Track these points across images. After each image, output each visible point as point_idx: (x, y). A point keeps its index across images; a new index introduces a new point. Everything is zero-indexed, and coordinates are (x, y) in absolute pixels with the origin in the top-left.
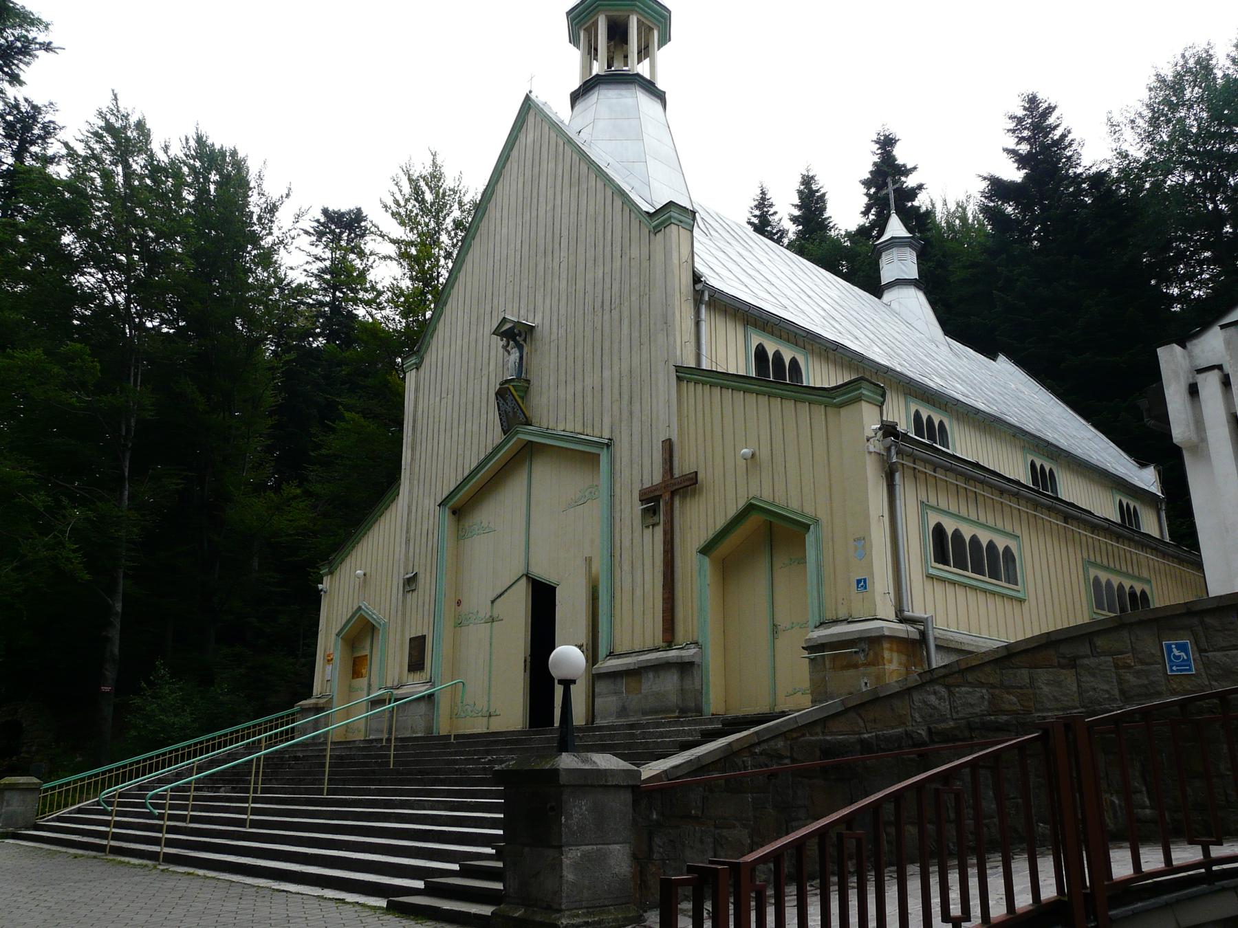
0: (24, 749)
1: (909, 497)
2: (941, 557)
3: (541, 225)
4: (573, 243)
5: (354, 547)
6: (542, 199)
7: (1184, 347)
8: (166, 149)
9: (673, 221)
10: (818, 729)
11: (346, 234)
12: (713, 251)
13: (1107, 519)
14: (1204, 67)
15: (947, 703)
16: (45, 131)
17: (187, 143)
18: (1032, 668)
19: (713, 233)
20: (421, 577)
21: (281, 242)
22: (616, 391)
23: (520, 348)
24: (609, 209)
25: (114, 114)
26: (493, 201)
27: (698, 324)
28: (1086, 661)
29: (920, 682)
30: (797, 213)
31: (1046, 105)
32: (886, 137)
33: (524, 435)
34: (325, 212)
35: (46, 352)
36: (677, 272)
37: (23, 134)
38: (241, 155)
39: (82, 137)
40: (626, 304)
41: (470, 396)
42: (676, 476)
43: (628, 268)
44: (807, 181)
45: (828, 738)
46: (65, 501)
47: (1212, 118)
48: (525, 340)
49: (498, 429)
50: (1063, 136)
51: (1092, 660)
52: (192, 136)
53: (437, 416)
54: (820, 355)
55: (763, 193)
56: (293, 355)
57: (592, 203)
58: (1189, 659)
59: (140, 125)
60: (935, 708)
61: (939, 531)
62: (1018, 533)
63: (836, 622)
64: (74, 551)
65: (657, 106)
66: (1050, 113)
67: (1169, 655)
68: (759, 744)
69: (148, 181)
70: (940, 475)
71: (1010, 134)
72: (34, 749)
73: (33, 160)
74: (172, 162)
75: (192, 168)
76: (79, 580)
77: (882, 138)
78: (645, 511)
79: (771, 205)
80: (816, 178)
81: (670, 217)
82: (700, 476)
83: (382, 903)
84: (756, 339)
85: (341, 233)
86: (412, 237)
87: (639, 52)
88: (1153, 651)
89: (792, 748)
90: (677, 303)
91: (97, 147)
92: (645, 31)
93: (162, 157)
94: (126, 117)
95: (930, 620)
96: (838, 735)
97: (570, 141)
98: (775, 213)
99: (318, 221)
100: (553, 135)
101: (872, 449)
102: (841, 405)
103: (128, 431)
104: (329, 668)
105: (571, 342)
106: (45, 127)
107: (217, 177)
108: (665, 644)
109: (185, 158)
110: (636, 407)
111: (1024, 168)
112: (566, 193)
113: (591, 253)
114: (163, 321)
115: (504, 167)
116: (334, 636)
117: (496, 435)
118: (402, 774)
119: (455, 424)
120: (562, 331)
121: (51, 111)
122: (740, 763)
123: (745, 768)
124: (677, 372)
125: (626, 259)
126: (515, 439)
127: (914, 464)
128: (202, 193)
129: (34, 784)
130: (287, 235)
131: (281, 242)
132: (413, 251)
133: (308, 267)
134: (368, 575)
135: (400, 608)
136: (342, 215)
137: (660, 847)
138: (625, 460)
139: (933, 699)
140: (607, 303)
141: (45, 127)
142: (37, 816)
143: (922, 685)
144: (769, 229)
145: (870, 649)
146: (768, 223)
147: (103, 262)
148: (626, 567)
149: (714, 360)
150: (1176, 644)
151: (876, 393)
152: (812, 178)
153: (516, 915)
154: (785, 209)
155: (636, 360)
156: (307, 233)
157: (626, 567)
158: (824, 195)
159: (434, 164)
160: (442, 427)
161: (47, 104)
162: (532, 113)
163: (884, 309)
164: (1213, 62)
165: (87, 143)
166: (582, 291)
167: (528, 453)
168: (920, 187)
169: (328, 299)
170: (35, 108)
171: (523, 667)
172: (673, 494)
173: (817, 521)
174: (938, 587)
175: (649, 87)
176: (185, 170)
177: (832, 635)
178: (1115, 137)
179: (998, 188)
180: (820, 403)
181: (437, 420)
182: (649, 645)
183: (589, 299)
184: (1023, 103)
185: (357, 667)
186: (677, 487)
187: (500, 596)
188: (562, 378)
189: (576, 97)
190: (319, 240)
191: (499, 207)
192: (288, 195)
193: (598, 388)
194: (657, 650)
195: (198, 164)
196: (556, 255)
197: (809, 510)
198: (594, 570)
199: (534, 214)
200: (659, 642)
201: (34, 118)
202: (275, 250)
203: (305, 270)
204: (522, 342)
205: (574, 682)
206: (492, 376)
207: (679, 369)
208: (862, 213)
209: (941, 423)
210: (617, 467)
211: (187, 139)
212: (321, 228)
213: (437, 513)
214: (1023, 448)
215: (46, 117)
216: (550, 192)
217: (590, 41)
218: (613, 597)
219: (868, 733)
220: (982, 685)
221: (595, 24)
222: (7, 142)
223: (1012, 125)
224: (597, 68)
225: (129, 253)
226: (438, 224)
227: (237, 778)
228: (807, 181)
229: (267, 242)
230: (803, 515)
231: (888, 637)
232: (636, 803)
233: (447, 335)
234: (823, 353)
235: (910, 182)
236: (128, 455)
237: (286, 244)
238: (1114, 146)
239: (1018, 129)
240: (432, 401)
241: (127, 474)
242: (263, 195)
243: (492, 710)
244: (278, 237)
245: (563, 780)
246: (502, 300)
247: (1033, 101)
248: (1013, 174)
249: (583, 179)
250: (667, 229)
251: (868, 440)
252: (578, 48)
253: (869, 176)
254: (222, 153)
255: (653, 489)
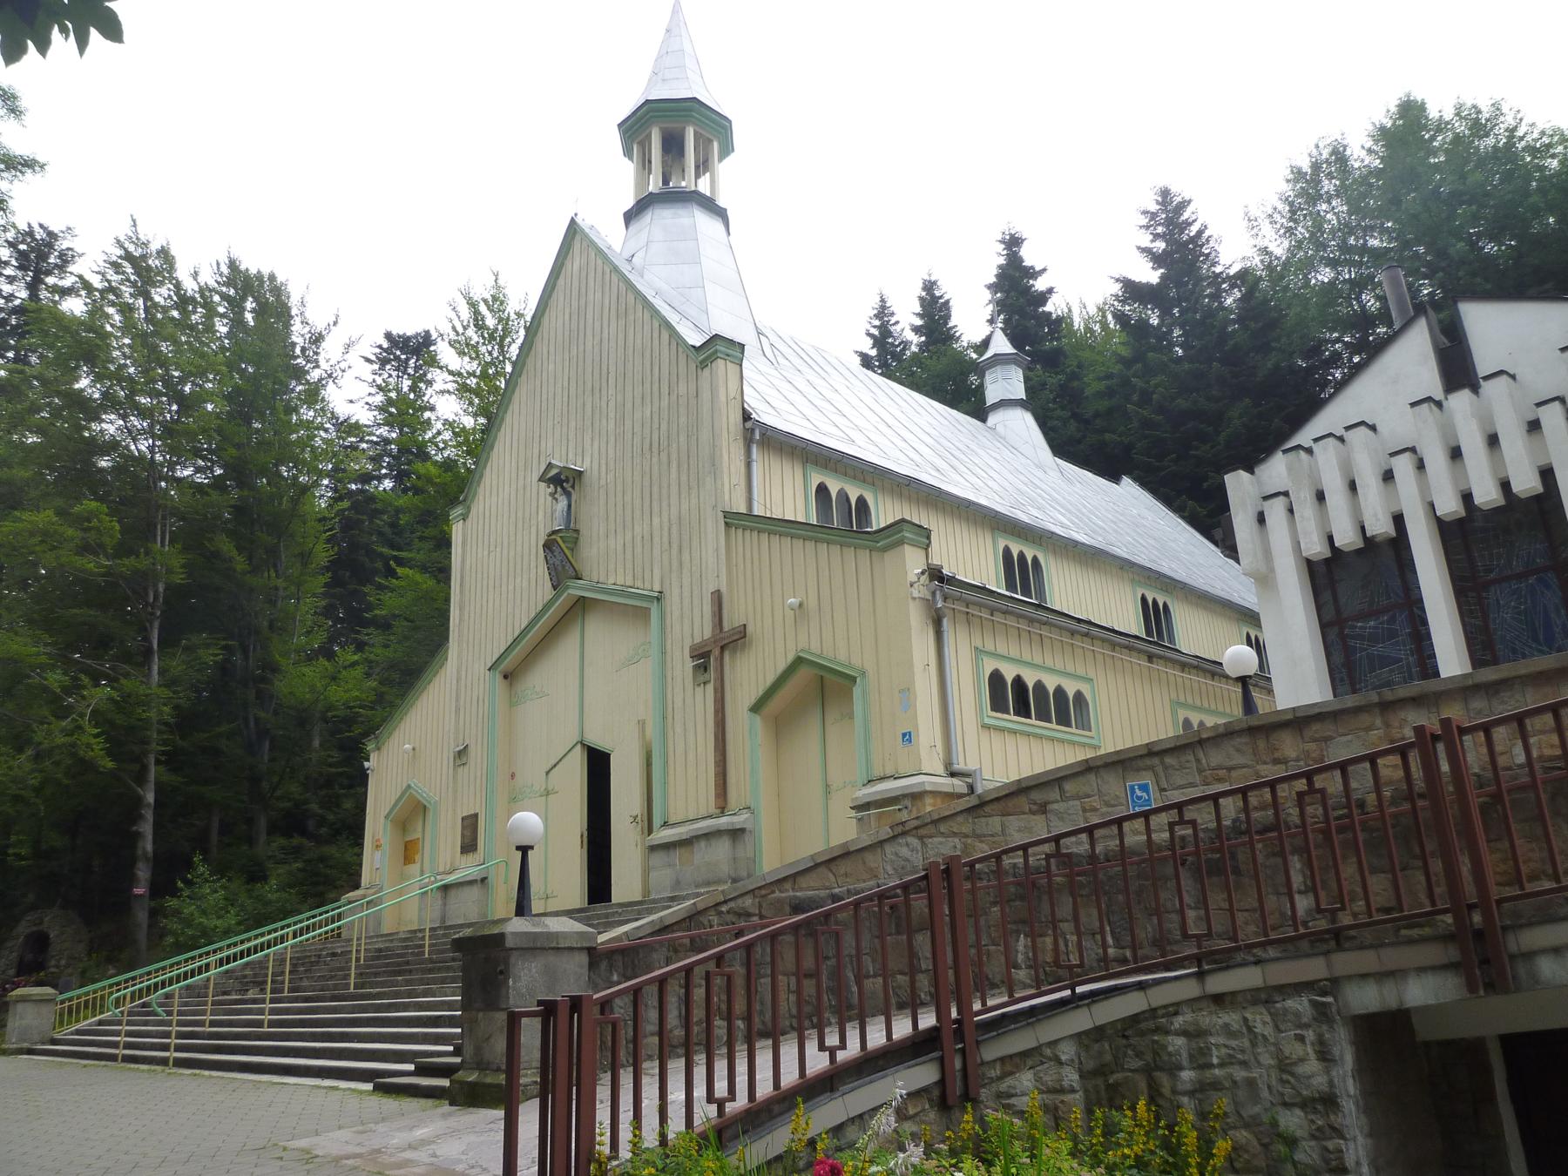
0: (53, 962)
1: (960, 644)
2: (998, 704)
3: (589, 362)
4: (620, 380)
5: (402, 719)
6: (589, 333)
7: (1252, 473)
8: (195, 275)
9: (719, 355)
10: (788, 885)
11: (413, 361)
12: (776, 382)
13: (1197, 657)
14: (1339, 156)
15: (920, 854)
16: (62, 260)
17: (218, 268)
18: (1004, 816)
19: (781, 359)
20: (472, 750)
21: (330, 376)
22: (665, 539)
23: (568, 495)
24: (656, 342)
25: (133, 242)
26: (539, 334)
27: (749, 465)
28: (1055, 806)
29: (891, 834)
30: (919, 322)
31: (1179, 199)
32: (1012, 236)
33: (575, 590)
34: (388, 336)
35: (61, 513)
36: (724, 411)
37: (37, 264)
38: (280, 279)
39: (97, 269)
40: (675, 445)
41: (519, 548)
42: (726, 629)
43: (675, 406)
44: (929, 286)
45: (798, 894)
46: (85, 680)
47: (1350, 213)
48: (573, 487)
49: (548, 584)
50: (1200, 233)
51: (1061, 804)
52: (224, 261)
53: (485, 572)
54: (892, 492)
55: (883, 301)
56: (346, 504)
57: (639, 336)
58: (1149, 800)
59: (164, 253)
60: (907, 860)
61: (996, 679)
62: (1091, 674)
63: (883, 779)
64: (96, 736)
65: (718, 225)
66: (1184, 207)
67: (1132, 796)
68: (725, 902)
69: (175, 314)
70: (998, 618)
71: (1143, 231)
72: (63, 962)
73: (49, 292)
74: (202, 290)
75: (224, 297)
76: (101, 769)
77: (1008, 237)
78: (696, 668)
79: (892, 314)
80: (938, 283)
81: (716, 351)
82: (750, 629)
83: (369, 1086)
84: (816, 479)
85: (407, 360)
86: (474, 366)
87: (697, 167)
88: (1117, 793)
89: (760, 906)
90: (725, 444)
91: (114, 278)
92: (703, 144)
93: (190, 286)
94: (145, 245)
95: (978, 772)
96: (808, 889)
97: (616, 269)
98: (897, 322)
99: (380, 347)
100: (600, 262)
101: (916, 594)
102: (885, 549)
103: (156, 598)
104: (378, 854)
105: (619, 488)
106: (62, 255)
107: (254, 305)
108: (718, 811)
109: (216, 285)
110: (686, 557)
111: (1160, 267)
112: (613, 324)
113: (638, 391)
114: (198, 470)
115: (550, 296)
116: (382, 819)
117: (547, 591)
118: (436, 963)
119: (505, 580)
120: (611, 477)
121: (69, 237)
122: (706, 923)
123: (711, 927)
124: (725, 517)
125: (674, 397)
126: (565, 594)
127: (968, 608)
128: (237, 322)
129: (49, 994)
130: (337, 367)
131: (330, 376)
132: (472, 382)
133: (370, 400)
134: (417, 749)
135: (451, 785)
136: (407, 339)
137: (621, 1008)
138: (676, 614)
139: (904, 851)
140: (655, 445)
141: (62, 255)
142: (54, 1029)
143: (894, 837)
144: (890, 340)
145: (913, 806)
146: (890, 334)
147: (124, 408)
148: (679, 729)
149: (768, 506)
150: (1138, 785)
151: (921, 536)
152: (935, 283)
153: (470, 1079)
154: (906, 318)
155: (685, 506)
156: (368, 360)
157: (679, 729)
158: (947, 302)
159: (497, 286)
160: (491, 583)
161: (64, 229)
162: (578, 238)
163: (986, 434)
164: (1348, 153)
165: (103, 275)
166: (631, 432)
167: (581, 607)
168: (1050, 291)
169: (394, 435)
170: (51, 234)
171: (579, 843)
172: (723, 648)
173: (863, 673)
174: (996, 737)
175: (710, 205)
176: (216, 298)
177: (876, 792)
178: (1253, 232)
179: (1133, 291)
180: (865, 547)
181: (485, 575)
182: (703, 813)
183: (637, 440)
184: (1156, 197)
185: (409, 853)
186: (726, 642)
187: (555, 766)
188: (612, 527)
189: (630, 217)
190: (382, 368)
191: (545, 341)
192: (335, 323)
193: (647, 537)
194: (710, 817)
195: (232, 292)
196: (604, 392)
197: (856, 661)
198: (648, 737)
199: (581, 348)
200: (712, 810)
201: (50, 246)
202: (323, 385)
203: (367, 403)
204: (570, 489)
205: (532, 848)
206: (541, 526)
207: (726, 514)
208: (988, 321)
209: (1035, 559)
210: (668, 621)
211: (218, 264)
212: (385, 354)
213: (487, 678)
214: (1132, 581)
215: (63, 244)
216: (597, 324)
217: (644, 154)
218: (666, 763)
219: (839, 887)
220: (955, 834)
221: (649, 136)
222: (20, 274)
223: (1144, 221)
224: (654, 184)
225: (154, 394)
226: (502, 351)
227: (254, 979)
228: (929, 286)
229: (315, 375)
230: (850, 666)
231: (931, 792)
232: (593, 965)
233: (494, 482)
234: (895, 487)
235: (1040, 285)
236: (156, 624)
237: (336, 378)
238: (1254, 242)
239: (1152, 226)
240: (480, 555)
241: (155, 646)
242: (307, 323)
243: (549, 892)
244: (326, 371)
245: (509, 943)
246: (550, 444)
247: (1165, 193)
248: (1149, 275)
249: (631, 311)
250: (713, 364)
251: (911, 586)
252: (631, 158)
253: (995, 280)
254: (259, 276)
255: (704, 643)
